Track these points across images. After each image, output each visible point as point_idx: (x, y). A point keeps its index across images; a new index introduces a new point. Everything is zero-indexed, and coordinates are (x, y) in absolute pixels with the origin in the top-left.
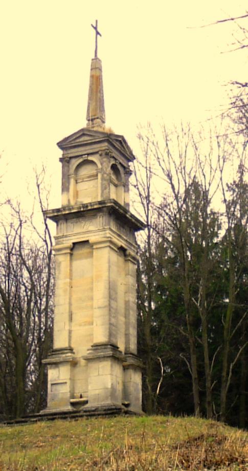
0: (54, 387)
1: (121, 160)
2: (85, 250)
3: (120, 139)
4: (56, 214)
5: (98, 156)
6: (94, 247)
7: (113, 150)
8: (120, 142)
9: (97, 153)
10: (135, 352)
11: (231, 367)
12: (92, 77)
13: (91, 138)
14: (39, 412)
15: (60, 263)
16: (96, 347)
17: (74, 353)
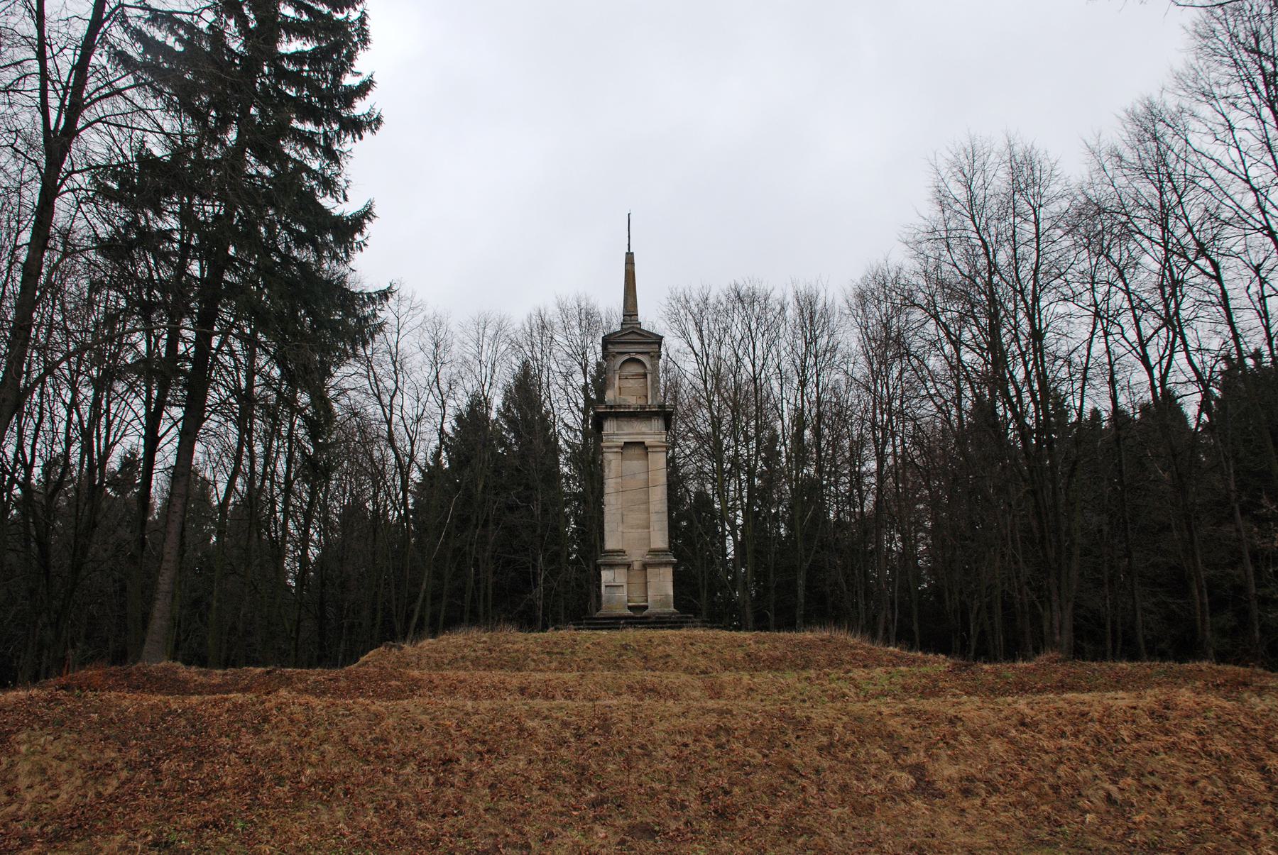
2: (637, 451)
9: (648, 353)
16: (654, 552)
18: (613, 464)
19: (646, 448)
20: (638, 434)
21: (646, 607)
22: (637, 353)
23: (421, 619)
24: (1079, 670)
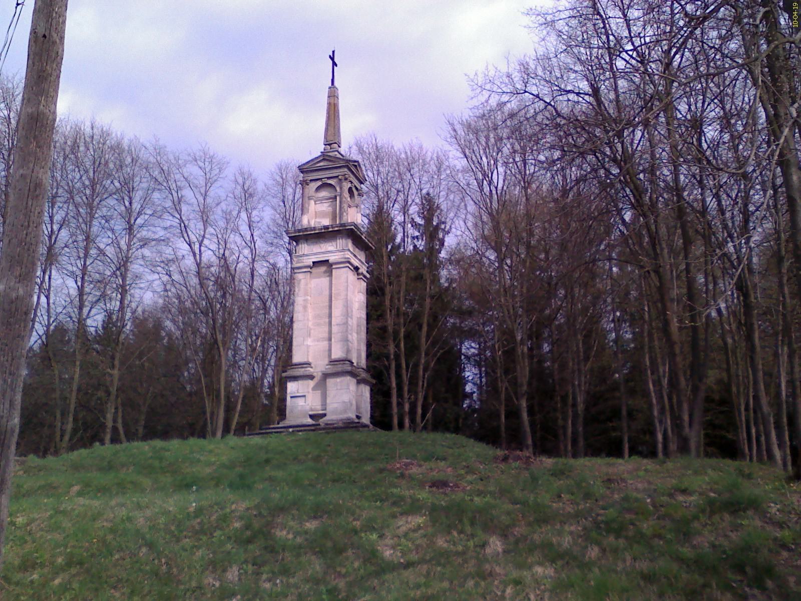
0: (293, 399)
1: (356, 183)
2: (323, 269)
3: (356, 164)
4: (297, 234)
5: (335, 180)
6: (334, 267)
7: (351, 176)
8: (355, 166)
9: (337, 177)
10: (365, 367)
11: (426, 376)
12: (329, 104)
13: (331, 163)
14: (278, 424)
15: (300, 280)
16: (333, 362)
17: (421, 431)
18: (303, 282)
19: (331, 265)
20: (323, 253)
21: (325, 415)
22: (329, 178)
23: (115, 429)
24: (587, 463)
